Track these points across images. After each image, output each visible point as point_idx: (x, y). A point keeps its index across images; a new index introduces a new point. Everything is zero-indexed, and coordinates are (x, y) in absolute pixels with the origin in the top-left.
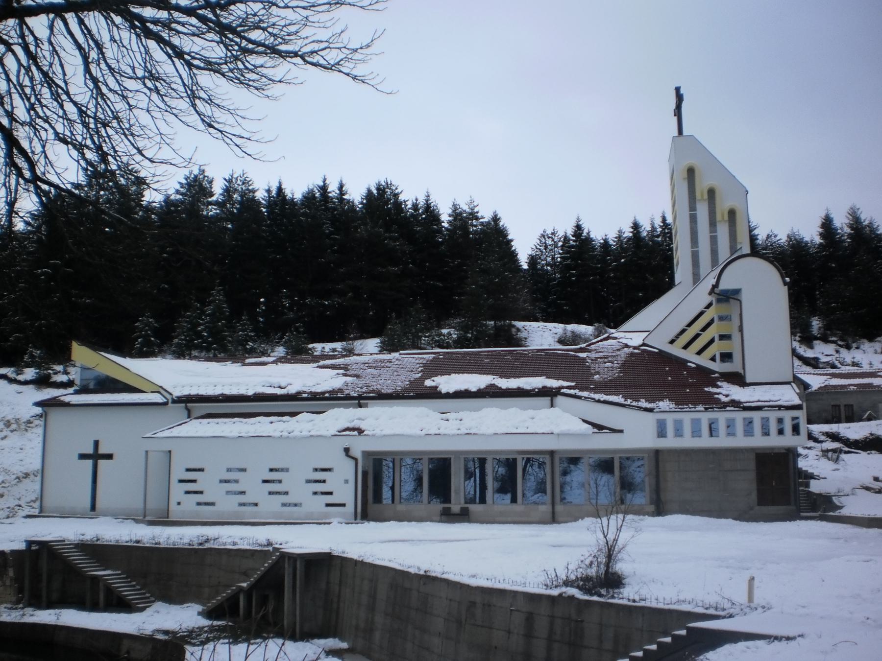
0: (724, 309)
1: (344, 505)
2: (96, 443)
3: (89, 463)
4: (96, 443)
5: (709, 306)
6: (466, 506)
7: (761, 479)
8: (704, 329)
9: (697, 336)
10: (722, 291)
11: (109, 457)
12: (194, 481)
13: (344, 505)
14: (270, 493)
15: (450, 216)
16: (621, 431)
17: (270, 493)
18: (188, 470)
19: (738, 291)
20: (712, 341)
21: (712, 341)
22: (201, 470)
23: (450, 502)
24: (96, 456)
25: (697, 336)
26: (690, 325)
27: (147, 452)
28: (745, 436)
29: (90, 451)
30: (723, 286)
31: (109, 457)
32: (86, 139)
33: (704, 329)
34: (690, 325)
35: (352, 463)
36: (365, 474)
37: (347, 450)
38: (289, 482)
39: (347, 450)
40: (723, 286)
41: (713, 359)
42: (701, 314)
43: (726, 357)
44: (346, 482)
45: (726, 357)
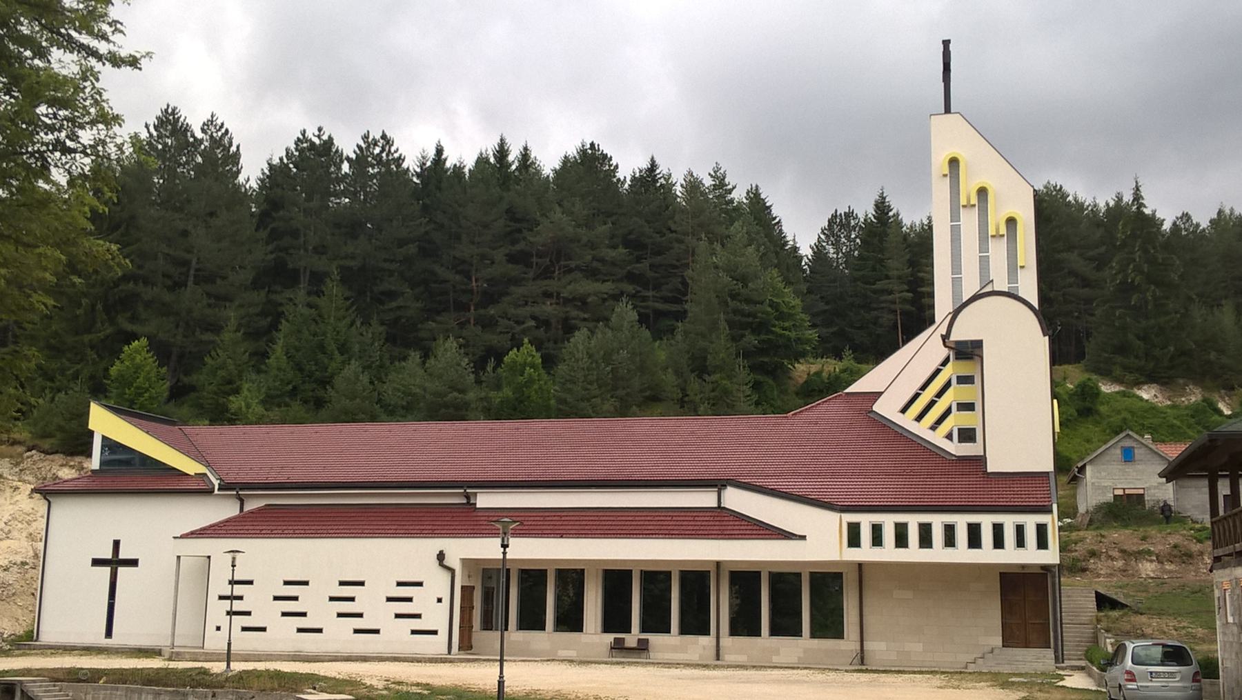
0: (965, 368)
1: (435, 632)
2: (117, 544)
3: (107, 570)
4: (117, 544)
5: (945, 363)
6: (644, 636)
7: (1008, 609)
8: (940, 394)
9: (932, 404)
10: (957, 343)
11: (133, 563)
12: (410, 600)
13: (435, 632)
14: (398, 616)
15: (1232, 210)
16: (803, 538)
17: (398, 616)
18: (342, 583)
19: (978, 344)
20: (948, 412)
21: (948, 412)
22: (420, 584)
23: (813, 636)
24: (115, 562)
25: (932, 404)
26: (924, 388)
27: (179, 557)
28: (921, 547)
29: (108, 555)
30: (954, 337)
31: (133, 563)
32: (55, 115)
33: (940, 394)
34: (924, 388)
35: (445, 577)
36: (467, 591)
37: (441, 556)
38: (308, 599)
39: (441, 556)
40: (954, 337)
41: (949, 437)
42: (938, 372)
43: (967, 435)
44: (440, 600)
45: (967, 435)
